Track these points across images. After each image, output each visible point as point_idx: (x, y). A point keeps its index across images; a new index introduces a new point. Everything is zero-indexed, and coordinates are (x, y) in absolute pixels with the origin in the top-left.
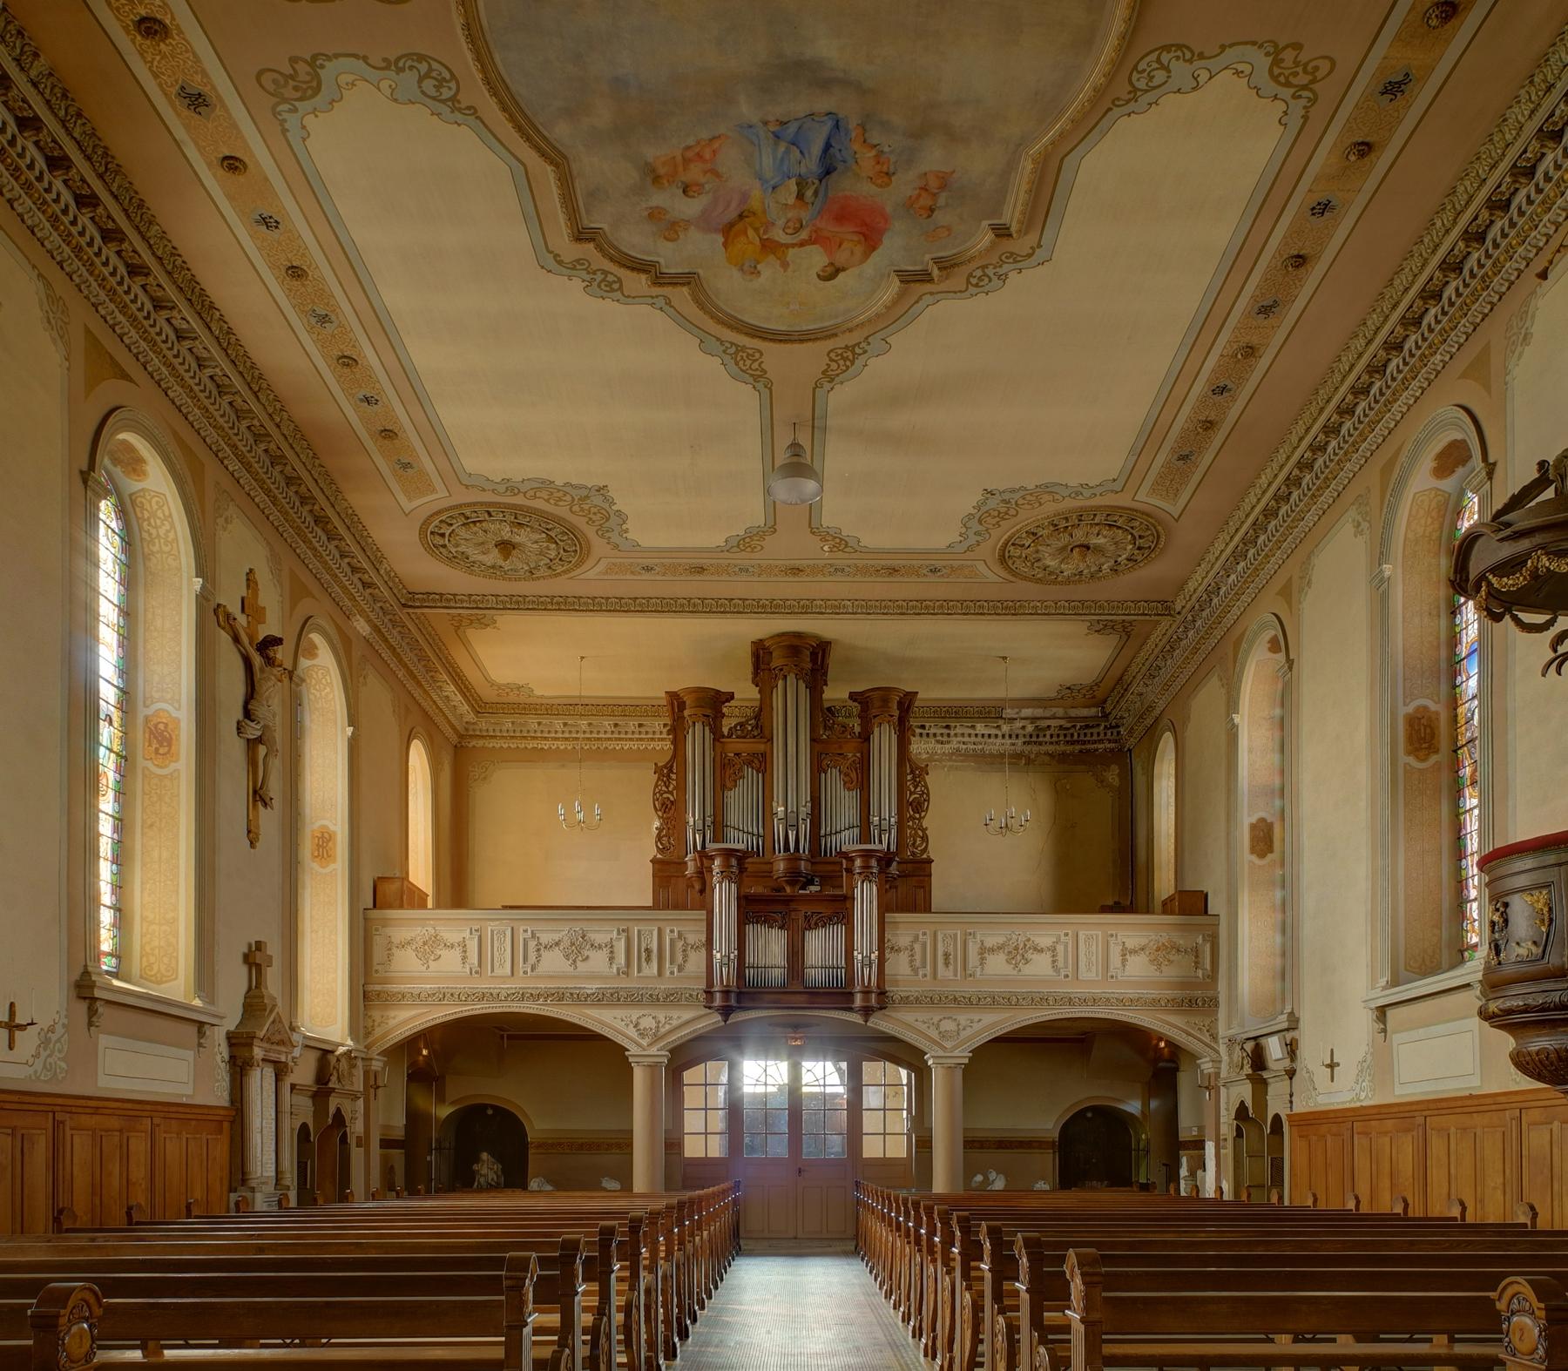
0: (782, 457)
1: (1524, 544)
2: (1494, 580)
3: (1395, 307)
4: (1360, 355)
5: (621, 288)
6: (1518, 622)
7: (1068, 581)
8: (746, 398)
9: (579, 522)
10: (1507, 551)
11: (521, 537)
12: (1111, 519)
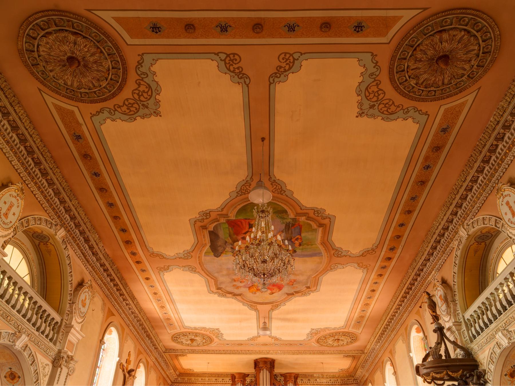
0: (262, 325)
7: (336, 347)
8: (254, 313)
9: (212, 335)
11: (197, 338)
12: (345, 334)
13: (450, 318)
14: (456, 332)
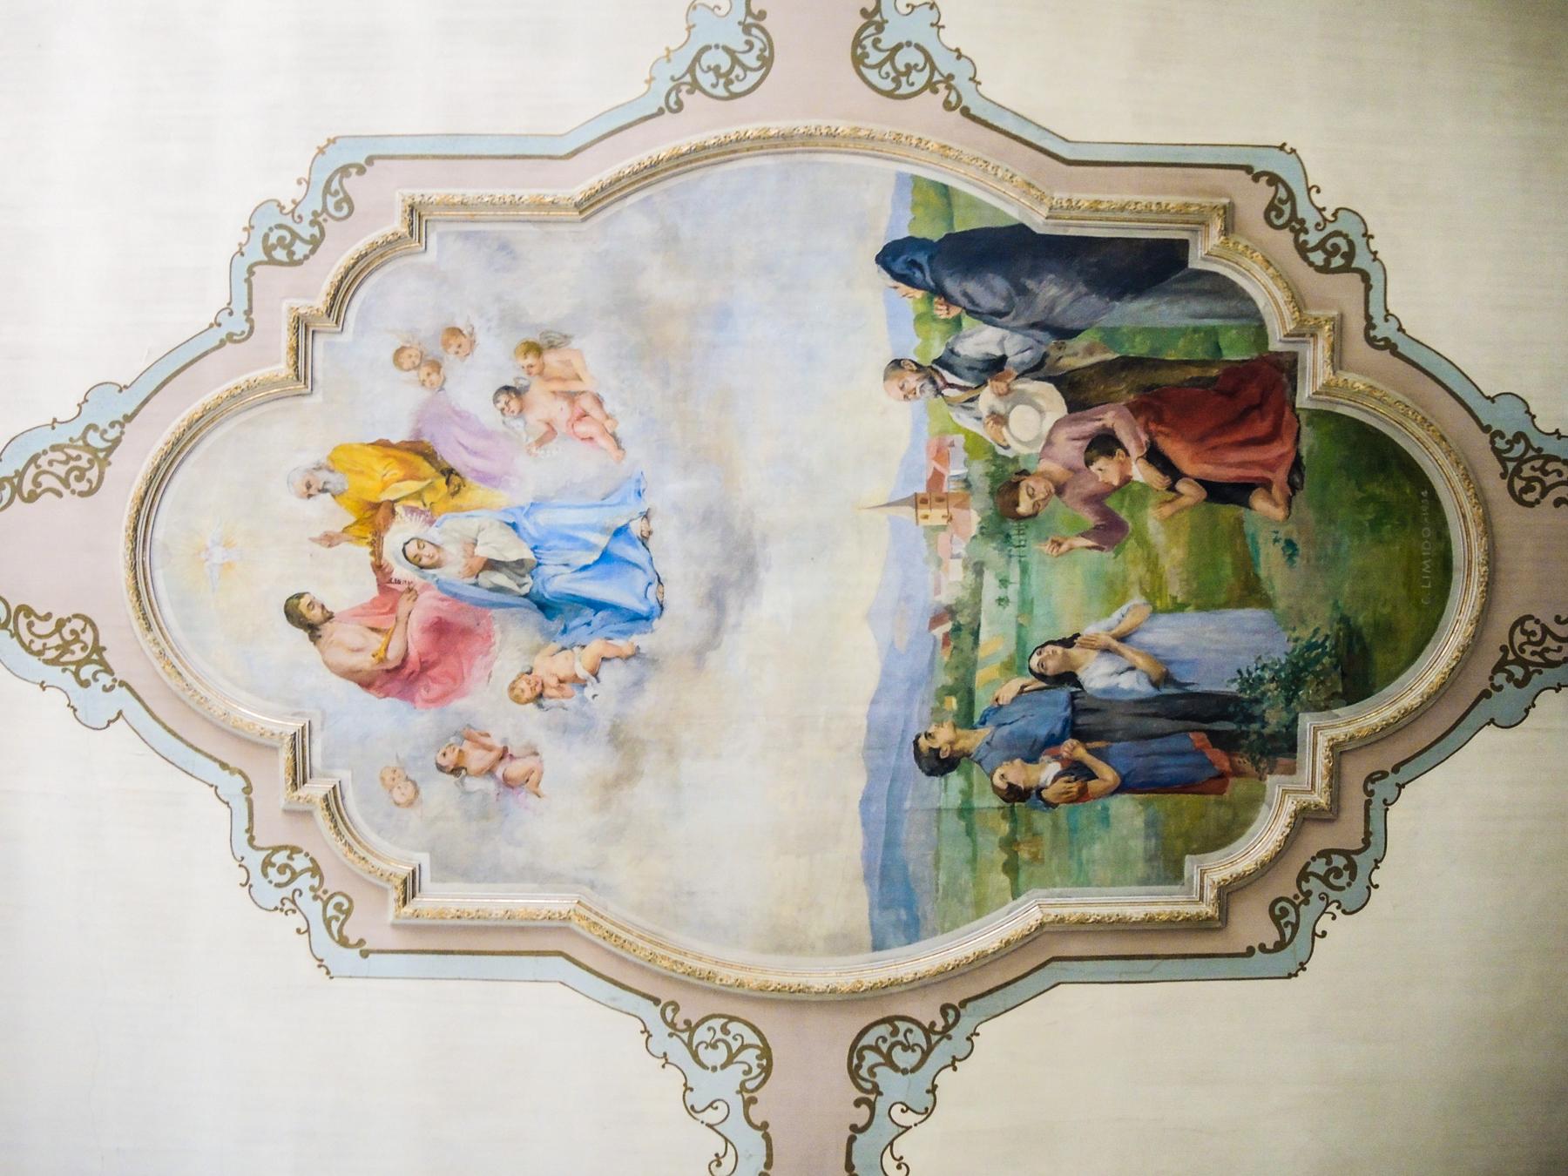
5: (1346, 854)
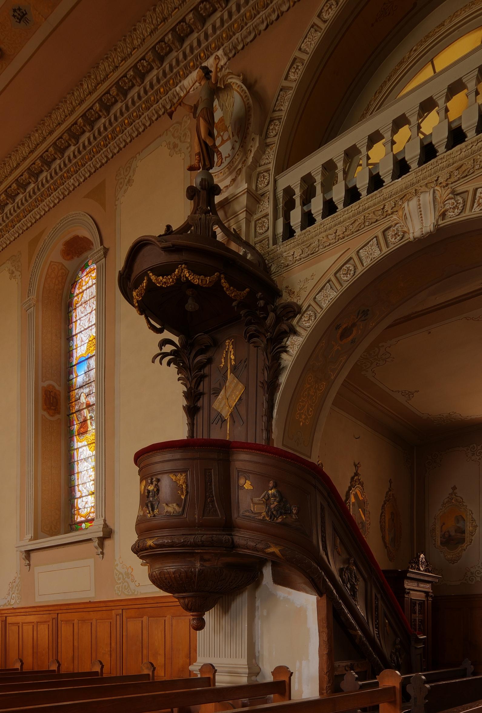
1: (175, 258)
2: (153, 278)
3: (51, 133)
4: (25, 159)
6: (149, 322)
10: (162, 258)
13: (234, 180)
14: (243, 216)
